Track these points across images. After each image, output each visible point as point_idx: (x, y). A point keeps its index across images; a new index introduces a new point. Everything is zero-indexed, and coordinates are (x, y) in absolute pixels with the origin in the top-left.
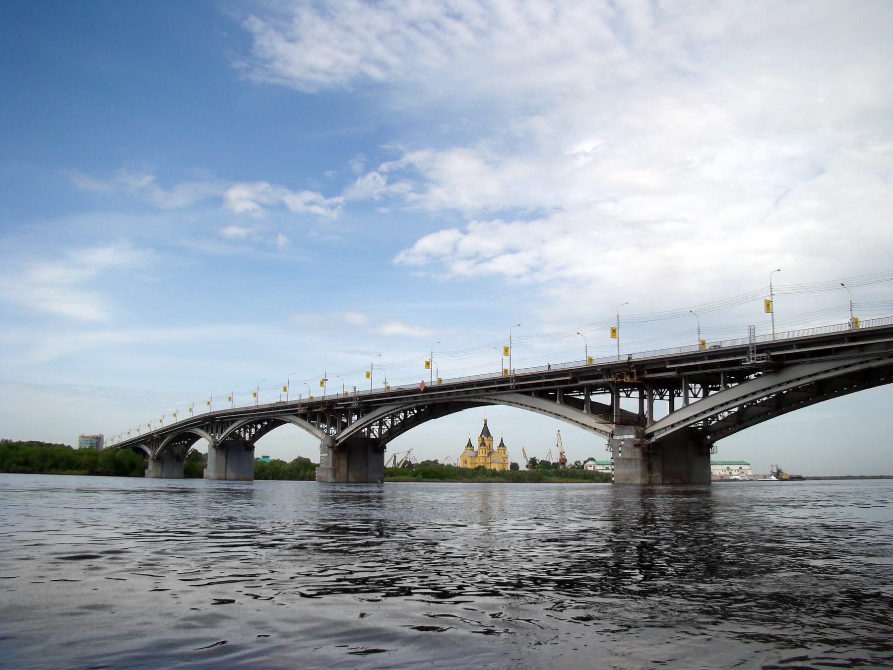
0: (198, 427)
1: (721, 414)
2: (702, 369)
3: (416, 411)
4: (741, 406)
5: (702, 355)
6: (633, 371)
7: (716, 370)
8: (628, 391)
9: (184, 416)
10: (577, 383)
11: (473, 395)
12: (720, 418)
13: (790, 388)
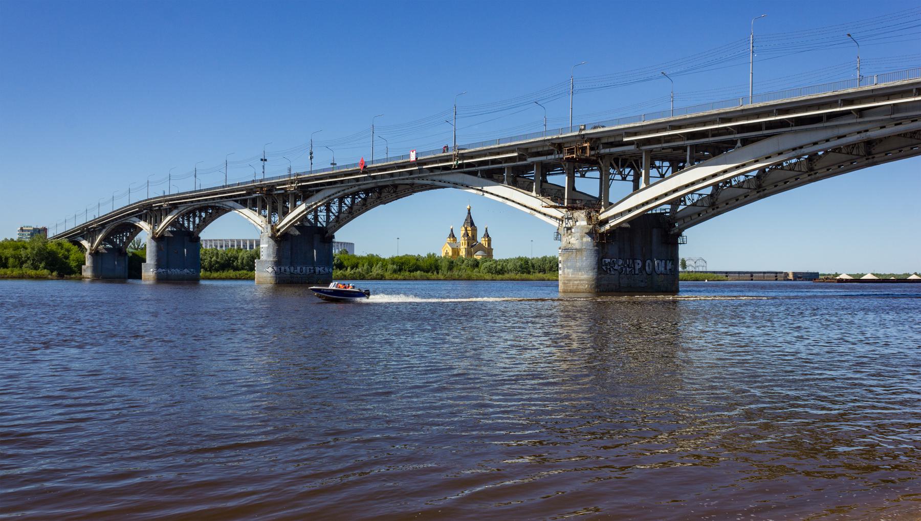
0: (136, 217)
1: (736, 178)
2: (713, 136)
3: (363, 196)
4: (715, 185)
5: (714, 117)
6: (586, 145)
7: (732, 136)
8: (583, 171)
9: (121, 203)
10: (525, 160)
11: (417, 176)
12: (689, 203)
13: (829, 148)
